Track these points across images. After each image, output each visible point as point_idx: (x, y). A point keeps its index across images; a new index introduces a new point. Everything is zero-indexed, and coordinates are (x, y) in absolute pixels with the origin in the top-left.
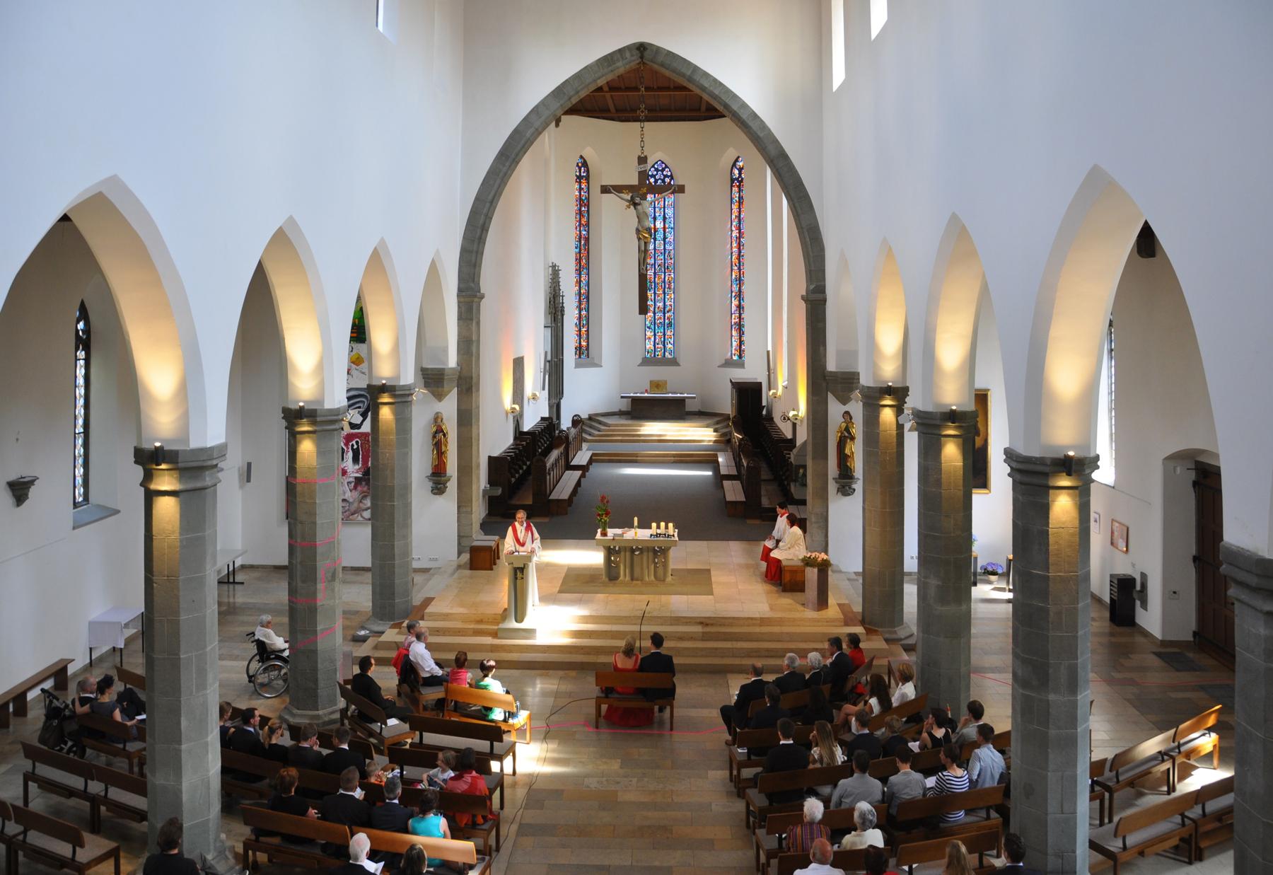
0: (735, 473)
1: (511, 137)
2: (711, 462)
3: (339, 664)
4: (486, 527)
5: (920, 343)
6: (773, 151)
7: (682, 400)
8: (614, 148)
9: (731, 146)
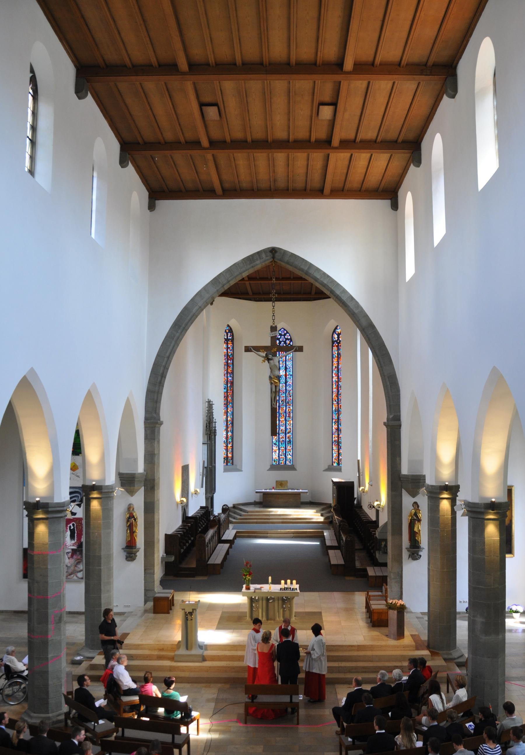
0: (336, 544)
1: (182, 312)
2: (319, 536)
3: (64, 680)
4: (164, 583)
5: (467, 454)
6: (364, 323)
7: (299, 494)
8: (254, 320)
9: (324, 317)
